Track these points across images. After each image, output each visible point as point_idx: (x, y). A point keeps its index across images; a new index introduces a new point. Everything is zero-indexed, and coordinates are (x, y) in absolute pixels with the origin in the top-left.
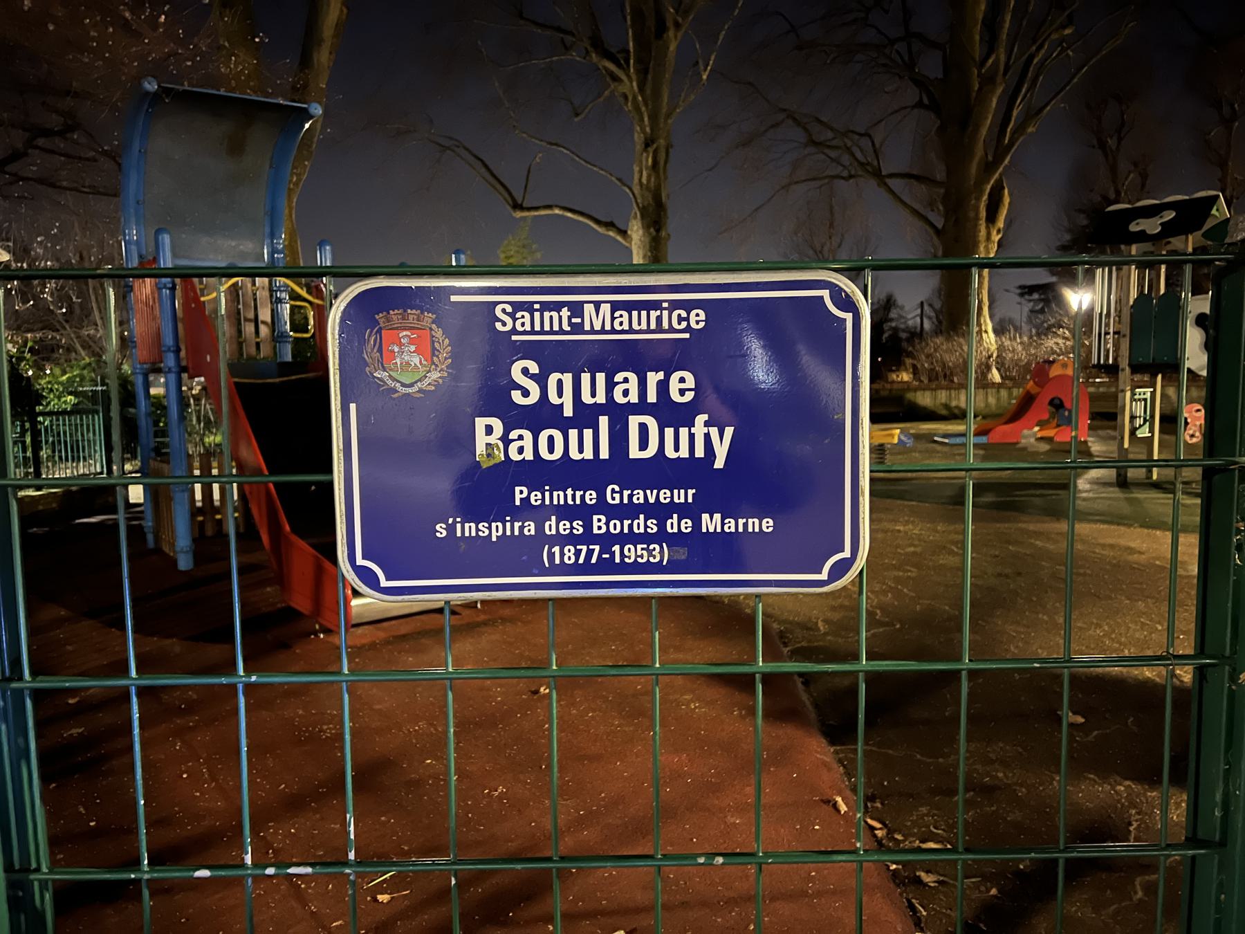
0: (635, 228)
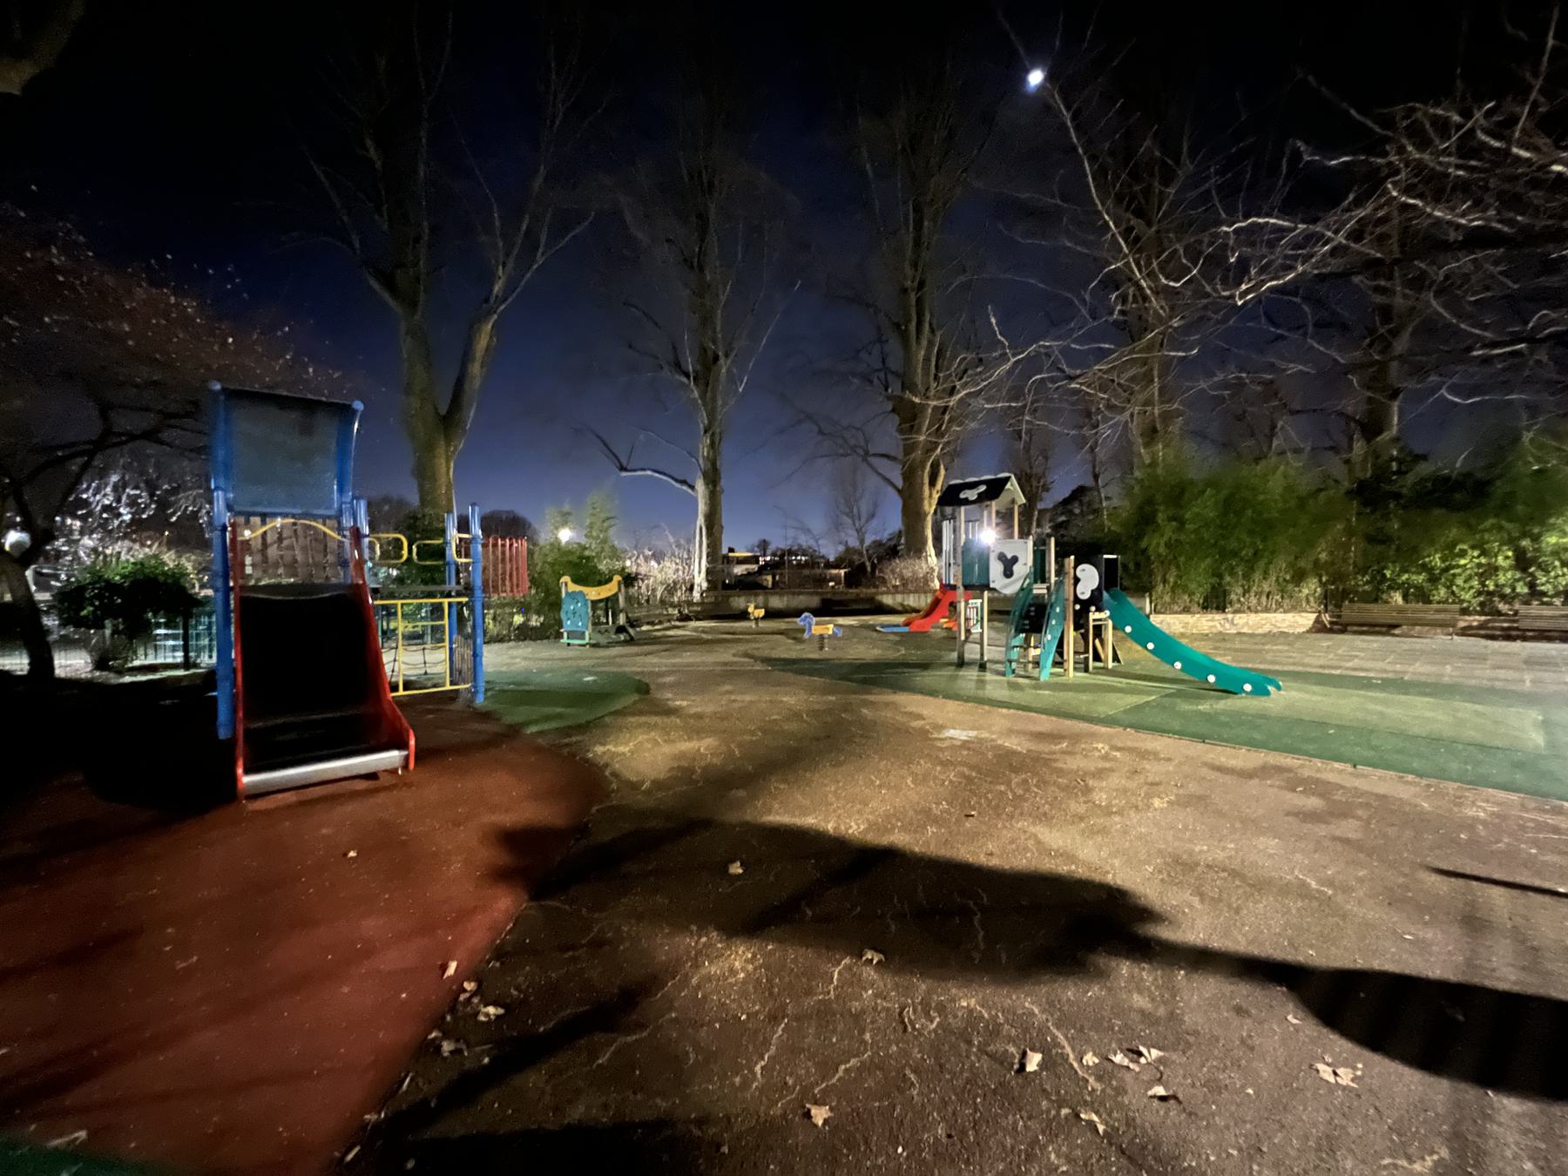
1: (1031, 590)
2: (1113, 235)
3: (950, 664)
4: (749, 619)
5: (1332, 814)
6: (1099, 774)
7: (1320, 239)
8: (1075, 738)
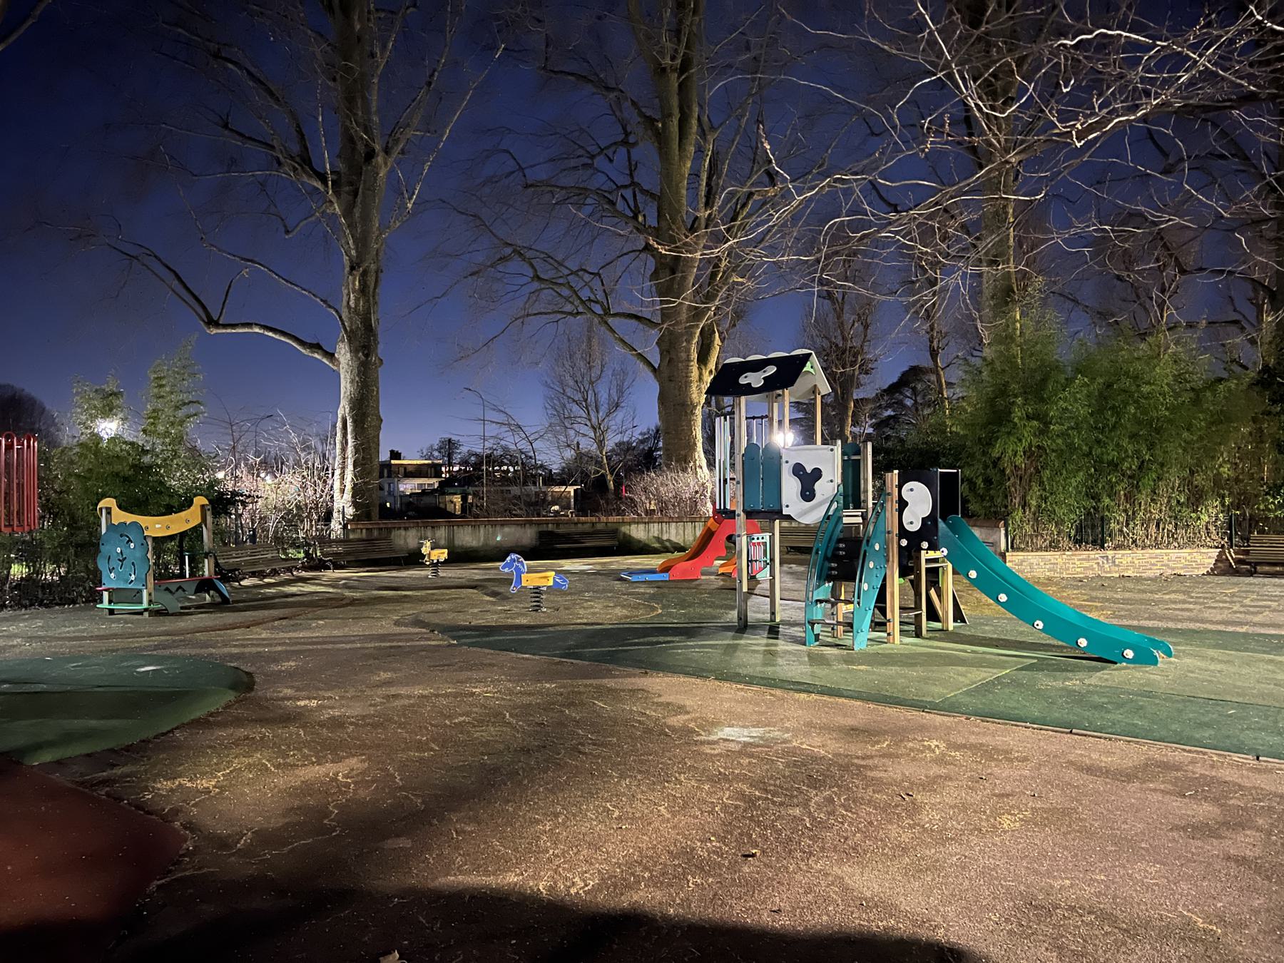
0: (343, 351)
1: (840, 518)
2: (931, 33)
3: (727, 628)
4: (423, 565)
5: (1226, 824)
6: (931, 785)
7: (1179, 62)
8: (900, 734)
